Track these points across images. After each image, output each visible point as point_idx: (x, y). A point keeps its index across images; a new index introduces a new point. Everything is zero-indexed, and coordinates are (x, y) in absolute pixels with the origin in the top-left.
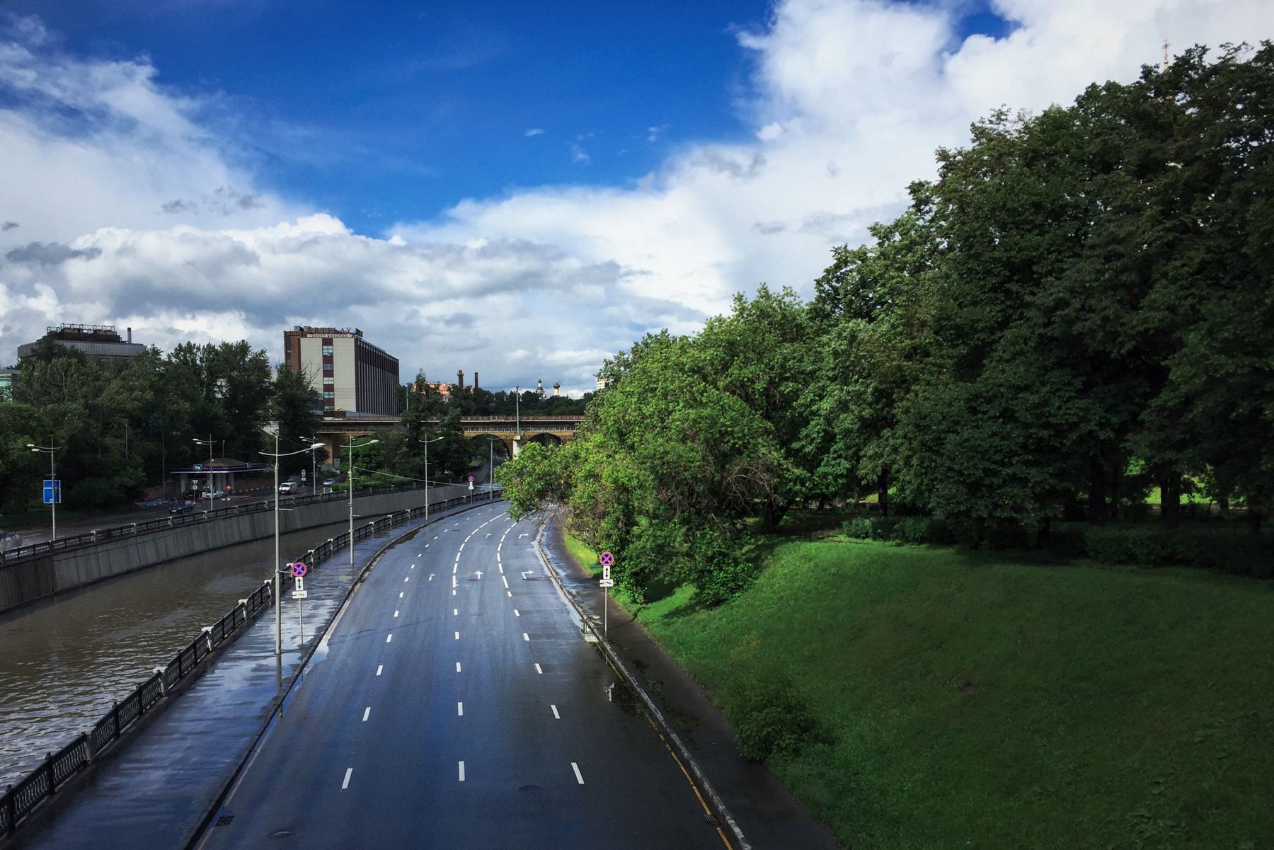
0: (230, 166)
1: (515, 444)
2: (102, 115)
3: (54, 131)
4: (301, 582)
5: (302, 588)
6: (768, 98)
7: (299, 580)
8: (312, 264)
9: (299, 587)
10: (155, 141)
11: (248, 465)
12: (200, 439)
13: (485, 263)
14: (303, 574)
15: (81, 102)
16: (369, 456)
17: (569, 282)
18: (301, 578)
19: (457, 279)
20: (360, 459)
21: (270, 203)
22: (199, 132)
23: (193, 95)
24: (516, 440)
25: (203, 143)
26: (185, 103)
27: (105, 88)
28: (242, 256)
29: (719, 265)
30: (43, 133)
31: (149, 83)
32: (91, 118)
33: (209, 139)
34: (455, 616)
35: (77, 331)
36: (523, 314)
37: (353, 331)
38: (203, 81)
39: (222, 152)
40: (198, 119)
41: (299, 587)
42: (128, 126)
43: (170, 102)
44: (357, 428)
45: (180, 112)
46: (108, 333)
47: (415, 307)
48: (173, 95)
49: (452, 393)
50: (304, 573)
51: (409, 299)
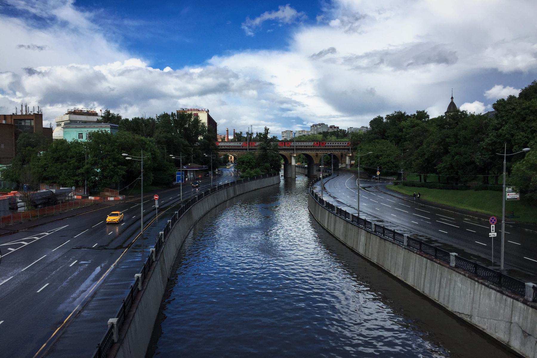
0: (108, 41)
1: (347, 158)
2: (53, 19)
3: (33, 26)
4: (494, 228)
5: (494, 231)
6: (338, 7)
7: (493, 227)
8: (127, 81)
9: (493, 231)
10: (76, 30)
11: (204, 166)
12: (174, 155)
13: (200, 81)
14: (495, 223)
15: (44, 15)
16: (249, 162)
17: (240, 90)
18: (494, 226)
19: (191, 87)
20: (245, 164)
21: (122, 55)
22: (96, 27)
23: (91, 11)
24: (294, 157)
25: (97, 31)
26: (87, 14)
27: (54, 7)
28: (100, 77)
29: (312, 81)
30: (29, 28)
31: (72, 6)
32: (48, 21)
33: (99, 29)
34: (474, 241)
35: (80, 111)
36: (223, 103)
37: (206, 110)
38: (95, 5)
39: (105, 35)
40: (94, 21)
41: (493, 231)
42: (64, 24)
43: (81, 14)
44: (225, 151)
45: (88, 19)
46: (93, 112)
47: (174, 99)
48: (82, 11)
49: (257, 135)
50: (495, 222)
51: (172, 97)
